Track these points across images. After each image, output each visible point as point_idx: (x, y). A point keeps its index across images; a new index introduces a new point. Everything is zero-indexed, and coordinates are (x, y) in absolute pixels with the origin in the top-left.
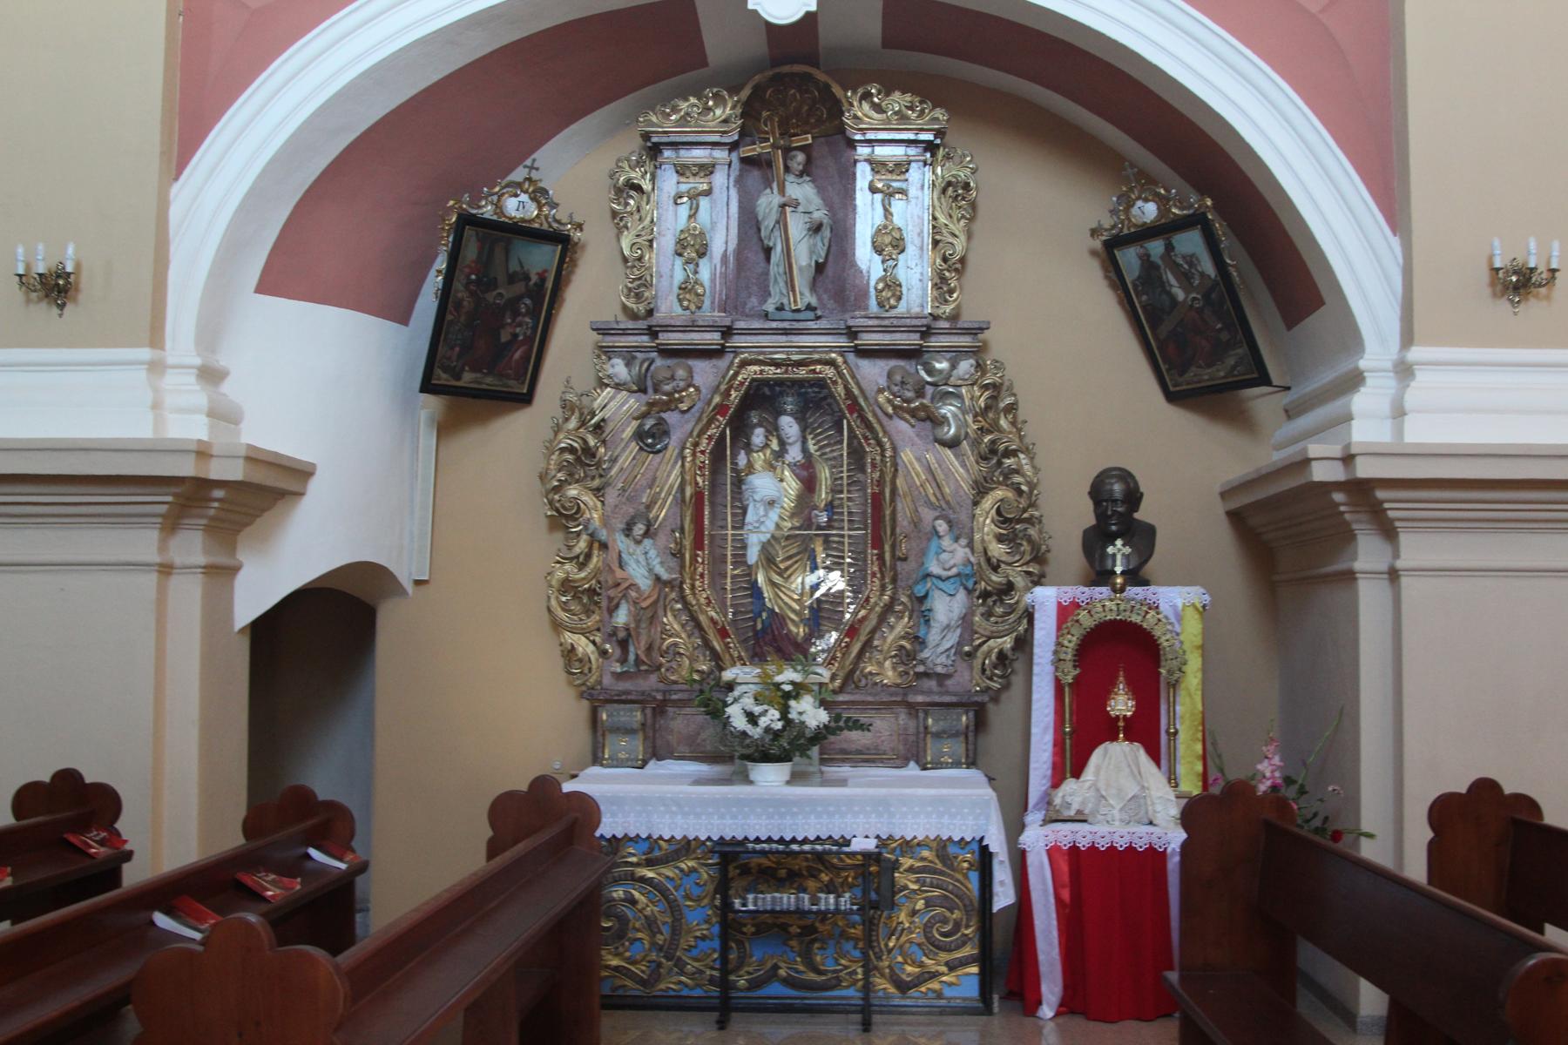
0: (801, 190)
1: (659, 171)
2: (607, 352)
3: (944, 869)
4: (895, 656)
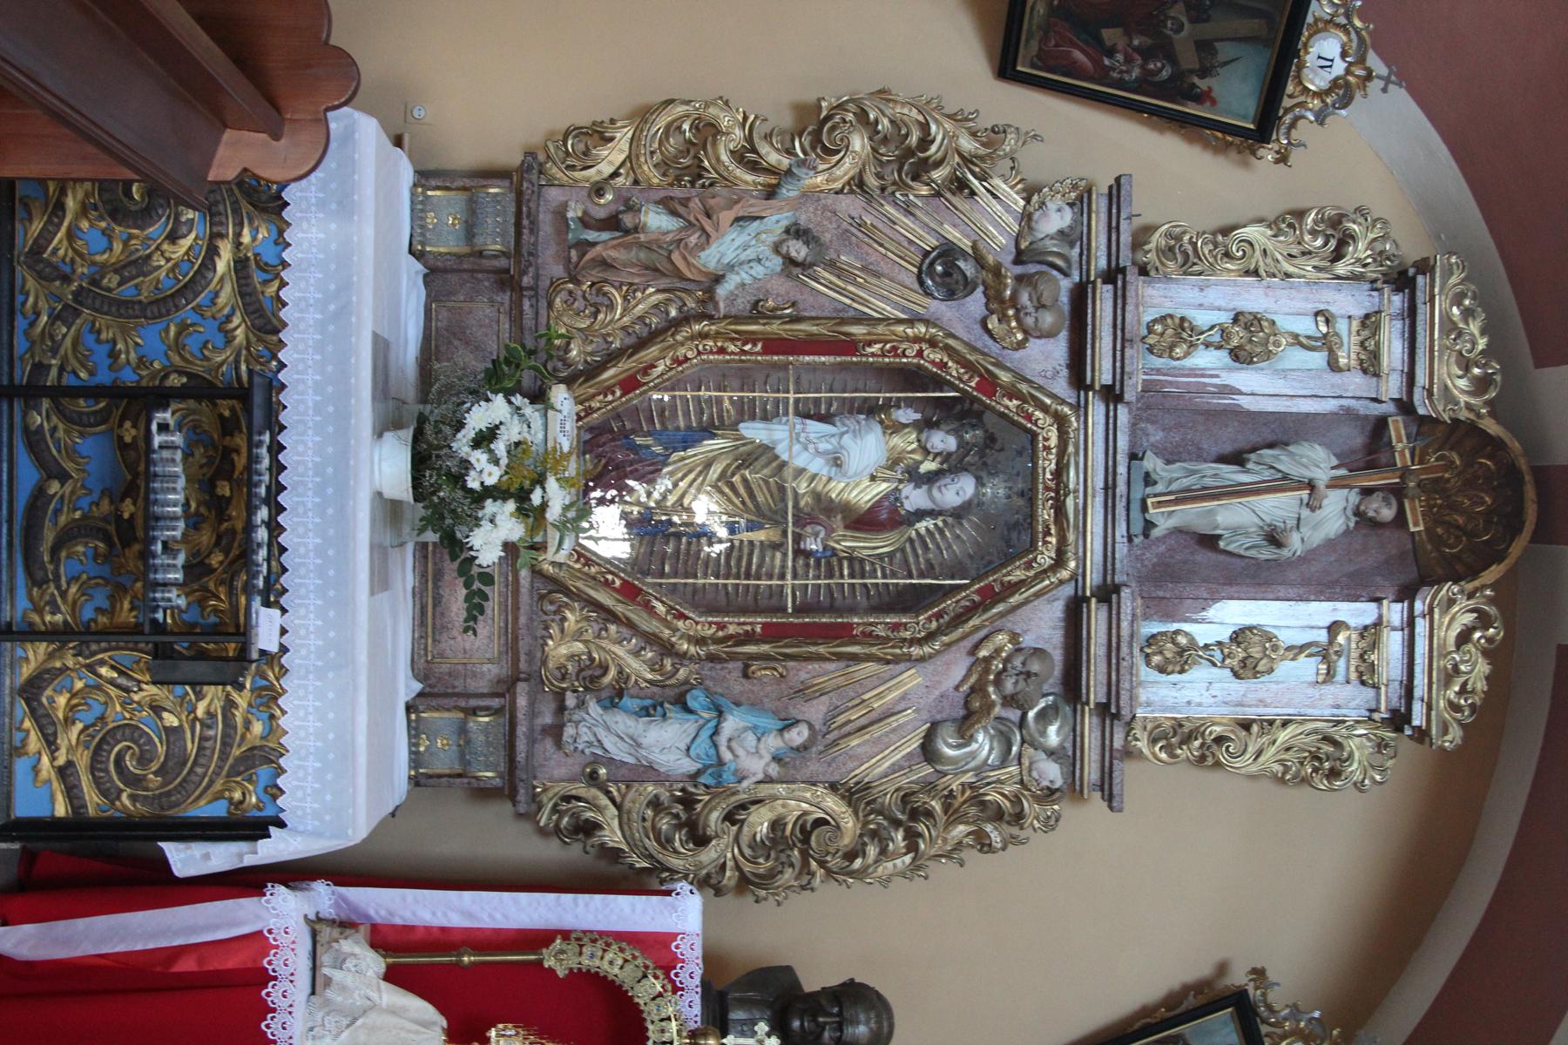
0: (1334, 513)
1: (1367, 286)
2: (1082, 201)
3: (231, 761)
4: (592, 659)
